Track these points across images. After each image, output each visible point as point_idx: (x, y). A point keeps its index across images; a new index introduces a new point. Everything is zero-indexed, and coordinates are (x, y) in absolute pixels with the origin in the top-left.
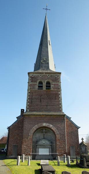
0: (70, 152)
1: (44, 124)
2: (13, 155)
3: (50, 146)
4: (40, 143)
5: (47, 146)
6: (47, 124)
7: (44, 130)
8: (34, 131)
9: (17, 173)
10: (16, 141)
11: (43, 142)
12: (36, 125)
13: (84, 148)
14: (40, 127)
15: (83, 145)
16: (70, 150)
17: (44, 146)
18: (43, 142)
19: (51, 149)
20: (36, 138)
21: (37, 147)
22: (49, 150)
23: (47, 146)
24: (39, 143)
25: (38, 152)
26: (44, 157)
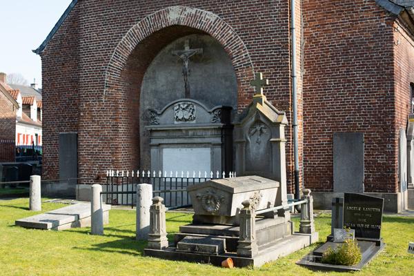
0: (331, 169)
1: (175, 15)
2: (65, 181)
3: (212, 136)
4: (167, 119)
5: (199, 133)
6: (189, 10)
7: (187, 48)
8: (126, 55)
9: (23, 275)
10: (71, 118)
11: (179, 114)
12: (132, 21)
13: (263, 140)
14: (152, 30)
15: (258, 122)
16: (331, 158)
17: (184, 137)
18: (180, 115)
19: (218, 150)
20: (156, 92)
21: (154, 142)
22: (212, 154)
23: (199, 133)
24: (161, 119)
25: (160, 168)
26: (179, 194)
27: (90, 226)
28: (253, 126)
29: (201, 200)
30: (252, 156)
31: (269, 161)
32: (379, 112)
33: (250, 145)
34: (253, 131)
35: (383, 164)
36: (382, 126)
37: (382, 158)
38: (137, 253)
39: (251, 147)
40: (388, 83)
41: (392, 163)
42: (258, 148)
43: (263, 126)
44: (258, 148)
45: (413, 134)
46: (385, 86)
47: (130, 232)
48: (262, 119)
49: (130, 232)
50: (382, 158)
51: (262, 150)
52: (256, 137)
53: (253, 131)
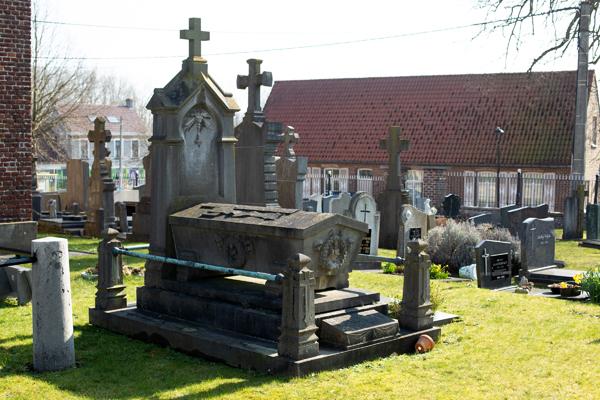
13: (207, 137)
15: (201, 106)
27: (29, 331)
28: (189, 114)
29: (322, 249)
30: (188, 169)
31: (214, 176)
32: (7, 88)
33: (186, 147)
34: (191, 121)
35: (13, 174)
36: (12, 113)
37: (12, 165)
38: (235, 380)
39: (185, 151)
40: (22, 42)
41: (27, 173)
42: (197, 154)
43: (205, 114)
44: (197, 154)
45: (590, 175)
46: (18, 46)
47: (25, 337)
48: (208, 102)
49: (25, 337)
50: (12, 165)
51: (203, 157)
52: (194, 133)
53: (191, 121)
